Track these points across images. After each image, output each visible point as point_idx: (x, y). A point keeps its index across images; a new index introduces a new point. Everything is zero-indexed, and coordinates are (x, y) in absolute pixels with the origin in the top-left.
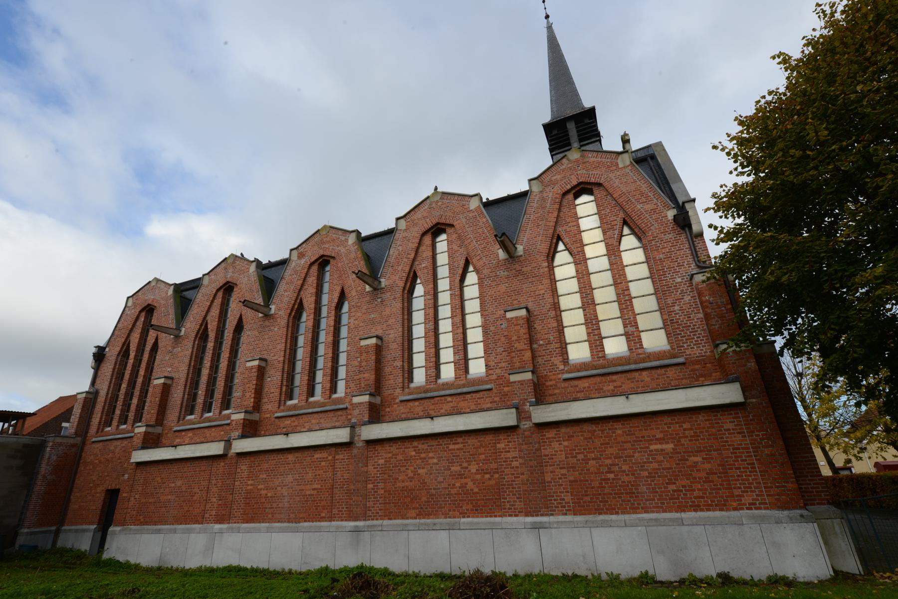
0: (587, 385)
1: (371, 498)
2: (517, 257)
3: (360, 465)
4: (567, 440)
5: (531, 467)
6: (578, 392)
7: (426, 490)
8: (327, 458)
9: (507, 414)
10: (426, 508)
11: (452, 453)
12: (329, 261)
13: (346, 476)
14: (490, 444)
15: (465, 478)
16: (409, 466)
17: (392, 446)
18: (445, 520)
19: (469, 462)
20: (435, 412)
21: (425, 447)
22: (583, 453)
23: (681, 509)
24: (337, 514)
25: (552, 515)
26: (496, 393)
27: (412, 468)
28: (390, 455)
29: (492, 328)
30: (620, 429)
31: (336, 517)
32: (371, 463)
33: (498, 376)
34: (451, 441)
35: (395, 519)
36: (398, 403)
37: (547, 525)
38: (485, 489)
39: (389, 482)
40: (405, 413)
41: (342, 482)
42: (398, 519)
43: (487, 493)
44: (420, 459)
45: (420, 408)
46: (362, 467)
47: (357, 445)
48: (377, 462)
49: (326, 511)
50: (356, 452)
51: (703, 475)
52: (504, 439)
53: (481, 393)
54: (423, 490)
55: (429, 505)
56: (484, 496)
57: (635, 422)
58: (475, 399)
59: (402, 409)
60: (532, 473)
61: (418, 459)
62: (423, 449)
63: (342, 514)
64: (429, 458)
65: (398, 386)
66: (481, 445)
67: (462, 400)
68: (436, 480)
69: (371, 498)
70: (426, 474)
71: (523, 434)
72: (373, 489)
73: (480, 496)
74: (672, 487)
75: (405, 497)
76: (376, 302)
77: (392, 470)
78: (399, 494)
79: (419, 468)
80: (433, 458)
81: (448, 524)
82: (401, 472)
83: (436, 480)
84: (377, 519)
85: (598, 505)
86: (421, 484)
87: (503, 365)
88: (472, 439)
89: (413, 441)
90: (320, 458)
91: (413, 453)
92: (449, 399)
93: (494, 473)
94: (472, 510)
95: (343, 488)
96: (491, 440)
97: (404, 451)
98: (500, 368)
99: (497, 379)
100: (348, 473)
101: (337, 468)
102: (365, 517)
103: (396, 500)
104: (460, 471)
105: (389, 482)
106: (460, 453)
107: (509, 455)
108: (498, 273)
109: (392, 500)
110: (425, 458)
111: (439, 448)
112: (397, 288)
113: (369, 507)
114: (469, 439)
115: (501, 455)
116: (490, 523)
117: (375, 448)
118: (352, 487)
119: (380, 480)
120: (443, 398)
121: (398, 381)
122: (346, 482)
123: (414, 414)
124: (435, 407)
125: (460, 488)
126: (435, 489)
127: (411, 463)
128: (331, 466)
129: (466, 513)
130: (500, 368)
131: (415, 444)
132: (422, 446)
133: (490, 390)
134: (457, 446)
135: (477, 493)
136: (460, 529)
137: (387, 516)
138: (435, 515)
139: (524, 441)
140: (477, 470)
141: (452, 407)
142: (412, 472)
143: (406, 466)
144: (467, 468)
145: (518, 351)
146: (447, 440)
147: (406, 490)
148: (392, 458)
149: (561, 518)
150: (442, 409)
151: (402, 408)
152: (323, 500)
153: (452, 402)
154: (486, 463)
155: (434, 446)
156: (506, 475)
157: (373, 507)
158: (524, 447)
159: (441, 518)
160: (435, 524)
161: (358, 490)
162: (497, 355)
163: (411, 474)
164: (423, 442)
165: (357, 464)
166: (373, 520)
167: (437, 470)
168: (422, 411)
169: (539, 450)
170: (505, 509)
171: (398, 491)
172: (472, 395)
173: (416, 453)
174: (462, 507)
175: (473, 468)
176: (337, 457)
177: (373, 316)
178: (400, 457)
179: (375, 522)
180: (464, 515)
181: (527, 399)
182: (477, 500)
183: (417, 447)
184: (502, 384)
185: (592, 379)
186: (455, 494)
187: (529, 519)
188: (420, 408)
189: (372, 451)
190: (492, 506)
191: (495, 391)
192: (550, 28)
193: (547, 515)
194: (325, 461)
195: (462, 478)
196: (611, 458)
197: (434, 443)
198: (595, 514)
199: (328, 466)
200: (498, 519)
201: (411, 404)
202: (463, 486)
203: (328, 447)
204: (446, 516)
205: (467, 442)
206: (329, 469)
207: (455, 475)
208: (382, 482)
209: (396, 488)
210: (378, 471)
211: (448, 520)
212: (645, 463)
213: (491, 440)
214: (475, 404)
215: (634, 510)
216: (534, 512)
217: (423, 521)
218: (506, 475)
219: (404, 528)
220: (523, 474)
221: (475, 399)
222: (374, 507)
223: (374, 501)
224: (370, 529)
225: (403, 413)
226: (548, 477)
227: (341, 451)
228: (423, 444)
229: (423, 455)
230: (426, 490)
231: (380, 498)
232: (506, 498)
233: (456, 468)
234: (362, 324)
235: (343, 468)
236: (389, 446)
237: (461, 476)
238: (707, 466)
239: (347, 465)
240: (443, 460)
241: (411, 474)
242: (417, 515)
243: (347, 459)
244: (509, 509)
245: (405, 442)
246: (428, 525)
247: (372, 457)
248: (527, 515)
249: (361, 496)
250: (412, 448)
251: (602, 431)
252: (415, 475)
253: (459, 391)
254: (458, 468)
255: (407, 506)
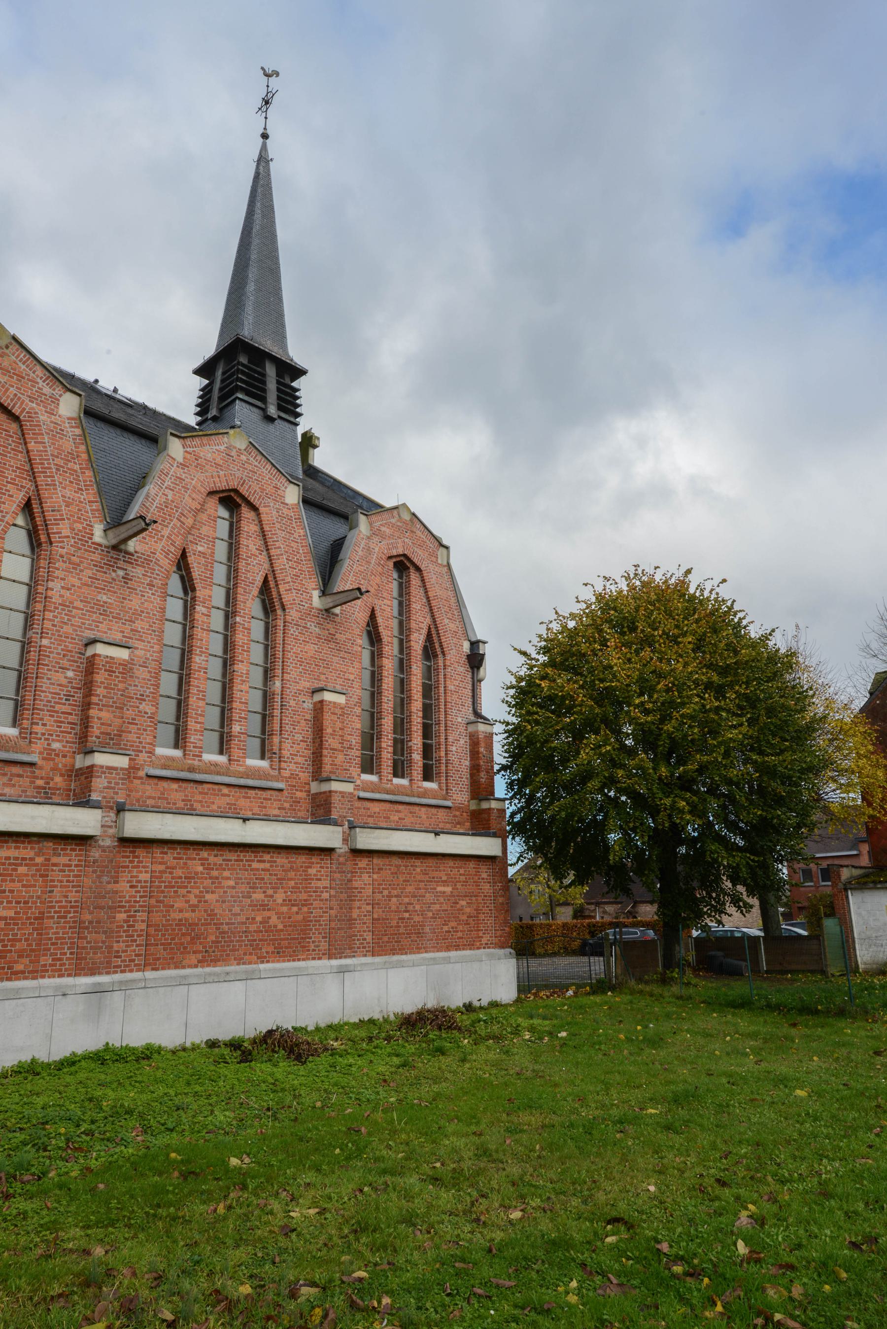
0: (377, 810)
1: (121, 937)
2: (333, 614)
3: (105, 879)
4: (377, 873)
5: (341, 900)
6: (369, 816)
7: (215, 924)
8: (31, 859)
9: (333, 832)
10: (214, 952)
11: (254, 875)
12: (240, 505)
13: (73, 896)
14: (301, 867)
15: (269, 910)
16: (192, 887)
17: (166, 853)
18: (237, 967)
19: (275, 888)
20: (203, 806)
21: (219, 860)
22: (388, 889)
23: (448, 949)
24: (51, 965)
25: (354, 956)
26: (287, 797)
27: (197, 891)
28: (162, 867)
29: (292, 703)
30: (420, 866)
31: (47, 971)
32: (125, 877)
33: (292, 774)
34: (256, 857)
35: (163, 969)
36: (141, 778)
37: (352, 968)
38: (290, 926)
39: (157, 912)
40: (154, 798)
41: (66, 907)
42: (169, 968)
43: (293, 931)
44: (211, 878)
45: (179, 796)
46: (109, 883)
47: (101, 843)
48: (137, 877)
49: (26, 961)
50: (97, 855)
51: (465, 918)
52: (317, 863)
53: (269, 792)
54: (210, 924)
55: (217, 947)
56: (289, 935)
57: (431, 862)
58: (260, 798)
59: (150, 789)
60: (341, 908)
61: (206, 878)
62: (215, 864)
63: (61, 965)
64: (223, 878)
65: (145, 747)
66: (292, 867)
67: (244, 797)
68: (230, 911)
69: (121, 937)
70: (217, 901)
71: (338, 860)
72: (125, 921)
73: (284, 935)
74: (446, 928)
75: (183, 934)
76: (114, 574)
77: (163, 892)
78: (174, 930)
79: (207, 892)
80: (229, 878)
81: (246, 972)
82: (178, 896)
83: (230, 911)
84: (131, 971)
85: (394, 946)
86: (209, 915)
87: (300, 759)
88: (282, 858)
89: (202, 850)
90: (16, 858)
91: (200, 869)
92: (225, 790)
93: (303, 905)
94: (273, 952)
95: (65, 917)
96: (304, 862)
97: (185, 864)
98: (295, 763)
99: (290, 778)
100: (76, 892)
101: (53, 881)
102: (108, 968)
103: (167, 939)
104: (263, 901)
105: (157, 912)
106: (265, 875)
107: (319, 884)
108: (309, 623)
109: (161, 939)
110: (217, 878)
111: (238, 865)
112: (157, 568)
113: (118, 952)
114: (277, 857)
115: (310, 883)
116: (295, 968)
117: (134, 852)
118: (87, 917)
119: (141, 906)
120: (216, 787)
121: (145, 739)
122: (72, 907)
123: (169, 803)
124: (204, 798)
125: (261, 923)
126: (227, 924)
127: (195, 883)
128: (41, 876)
129: (265, 957)
130: (295, 763)
131: (204, 854)
132: (213, 858)
133: (281, 790)
134: (262, 866)
135: (282, 930)
136: (260, 978)
137: (150, 964)
138: (224, 960)
139: (337, 868)
140: (284, 900)
141: (228, 804)
142: (196, 896)
143: (186, 887)
144: (272, 896)
145: (332, 749)
146: (250, 855)
147: (185, 925)
148: (165, 872)
149: (363, 960)
150: (213, 803)
151: (148, 787)
152: (20, 940)
153: (229, 796)
154: (296, 892)
155: (230, 860)
156: (314, 908)
157: (123, 951)
158: (337, 876)
159: (231, 965)
160: (228, 974)
161: (98, 922)
162: (294, 743)
163: (194, 901)
164: (216, 852)
165: (99, 877)
166: (123, 972)
167: (232, 897)
168: (183, 800)
169: (350, 881)
170: (309, 950)
171: (172, 925)
172: (257, 791)
173: (204, 869)
174: (261, 949)
175: (280, 897)
176: (55, 860)
177: (104, 598)
178: (179, 872)
179: (128, 976)
180: (262, 959)
181: (345, 817)
182: (281, 939)
183: (207, 859)
184: (295, 786)
185: (382, 804)
186: (255, 931)
187: (335, 962)
188: (179, 796)
189: (128, 857)
190: (297, 947)
191: (285, 793)
192: (263, 160)
193: (350, 957)
194: (26, 865)
195: (264, 910)
196: (408, 896)
197: (232, 856)
198: (390, 954)
199: (32, 876)
200: (302, 964)
201: (165, 784)
202: (265, 921)
203: (316, 853)
204: (240, 961)
205: (275, 862)
206: (36, 881)
207: (256, 906)
208: (143, 911)
209: (169, 920)
210: (136, 892)
211: (242, 967)
212: (432, 903)
213: (304, 862)
214: (259, 807)
215: (419, 950)
216: (339, 953)
217: (208, 970)
218: (314, 908)
219: (183, 982)
220: (331, 909)
221: (260, 798)
222: (126, 951)
223: (127, 941)
224: (124, 987)
225: (149, 797)
226: (355, 914)
227: (62, 849)
228: (216, 856)
229: (215, 873)
230: (215, 924)
231: (138, 936)
232: (311, 938)
233: (258, 896)
234: (78, 604)
235: (68, 881)
236: (162, 853)
237: (264, 907)
238: (468, 910)
239: (75, 876)
240: (242, 883)
241: (194, 901)
242: (199, 961)
243: (76, 866)
244: (314, 950)
245: (189, 849)
246: (218, 975)
247: (128, 867)
248: (330, 958)
249: (105, 932)
250: (200, 859)
251: (406, 866)
252: (199, 901)
253: (242, 782)
254: (262, 896)
255: (185, 948)
